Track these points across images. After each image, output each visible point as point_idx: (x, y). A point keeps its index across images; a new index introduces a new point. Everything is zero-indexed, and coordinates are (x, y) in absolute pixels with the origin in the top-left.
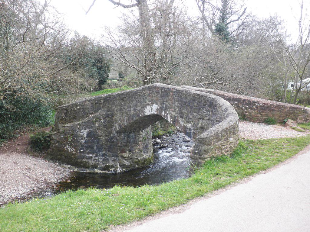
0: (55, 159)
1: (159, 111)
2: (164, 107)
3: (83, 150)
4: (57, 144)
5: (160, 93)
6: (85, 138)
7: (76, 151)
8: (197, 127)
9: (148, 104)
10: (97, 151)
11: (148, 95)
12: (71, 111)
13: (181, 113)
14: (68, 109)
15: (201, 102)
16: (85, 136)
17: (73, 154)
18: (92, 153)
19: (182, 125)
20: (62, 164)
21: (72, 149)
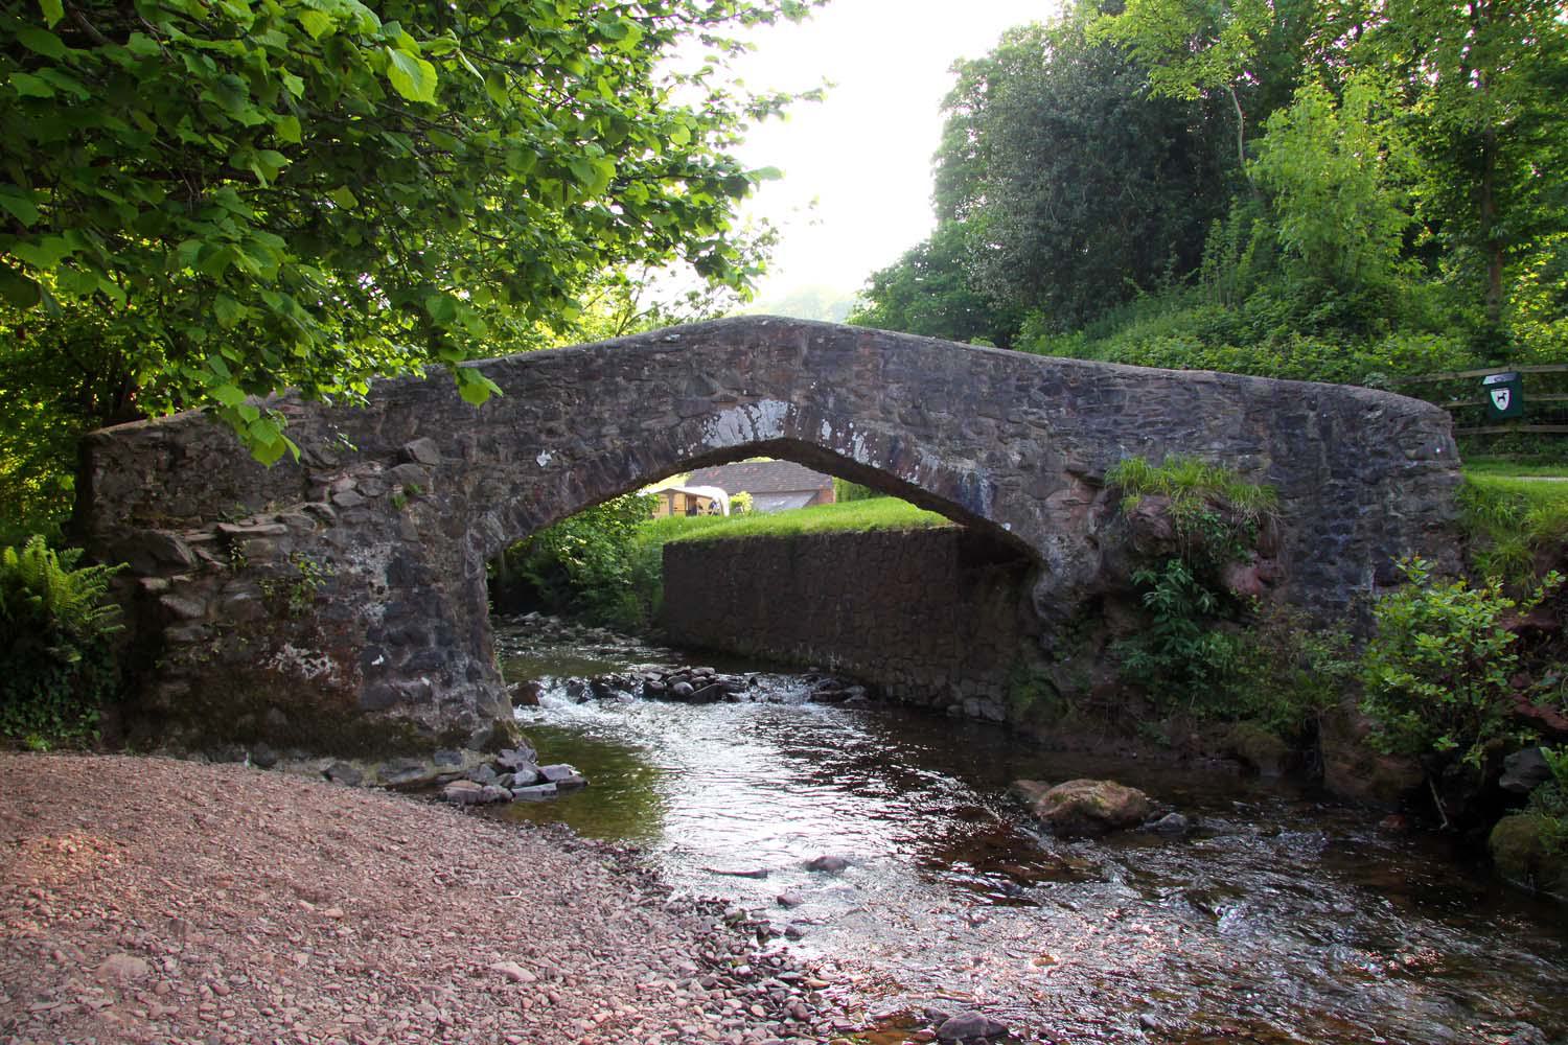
0: (226, 741)
1: (802, 424)
2: (831, 405)
3: (381, 659)
4: (216, 646)
5: (805, 350)
6: (381, 590)
7: (347, 673)
8: (1006, 466)
9: (729, 402)
10: (445, 656)
11: (729, 364)
12: (205, 453)
13: (925, 423)
14: (181, 440)
15: (1008, 378)
16: (380, 580)
17: (332, 690)
18: (429, 673)
19: (935, 468)
20: (282, 757)
21: (323, 664)
